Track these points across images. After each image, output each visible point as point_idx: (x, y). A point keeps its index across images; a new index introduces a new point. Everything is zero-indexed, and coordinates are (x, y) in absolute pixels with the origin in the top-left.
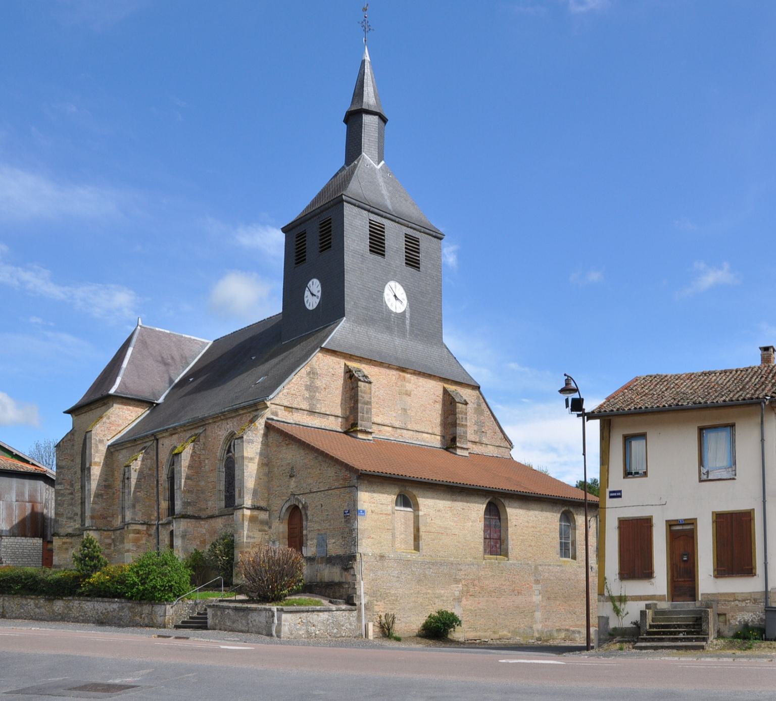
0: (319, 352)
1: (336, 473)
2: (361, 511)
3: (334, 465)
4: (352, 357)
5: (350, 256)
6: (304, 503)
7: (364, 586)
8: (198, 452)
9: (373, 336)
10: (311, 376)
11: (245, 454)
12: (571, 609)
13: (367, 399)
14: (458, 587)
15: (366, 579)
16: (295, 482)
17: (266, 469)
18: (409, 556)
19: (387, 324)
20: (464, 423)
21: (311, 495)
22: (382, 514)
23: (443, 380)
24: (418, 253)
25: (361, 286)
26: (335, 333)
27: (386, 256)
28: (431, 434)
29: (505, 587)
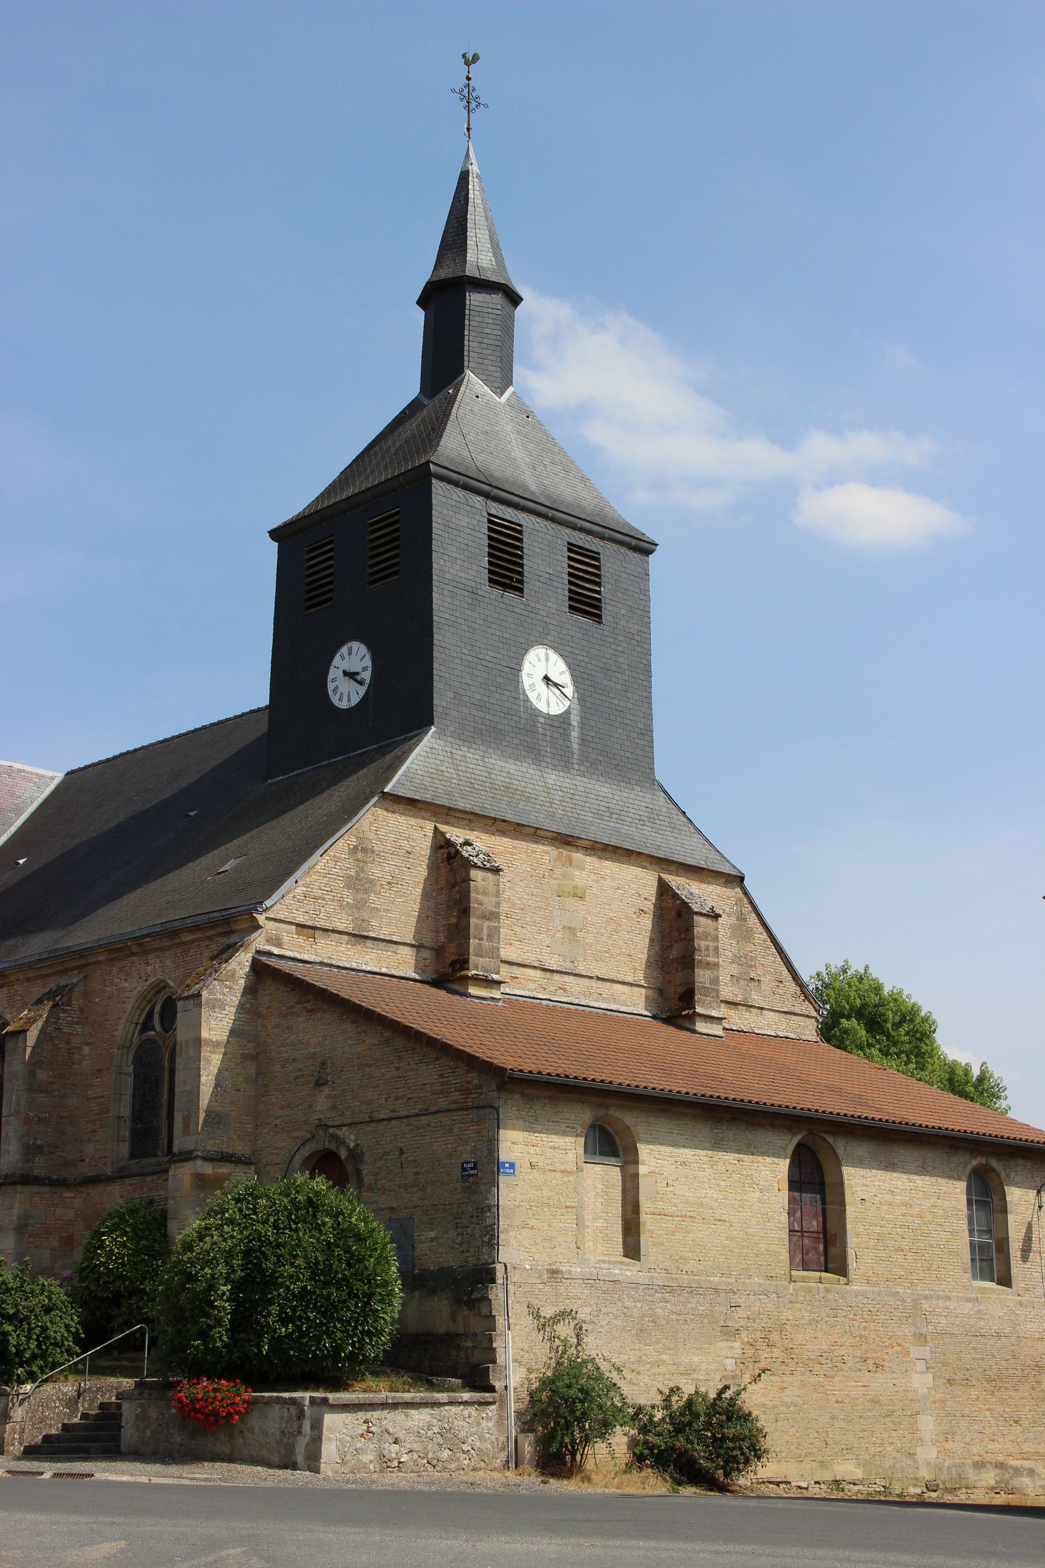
0: (374, 805)
1: (441, 1076)
2: (507, 1165)
3: (438, 1059)
4: (451, 813)
5: (446, 593)
6: (352, 1145)
7: (514, 1342)
8: (66, 1030)
9: (496, 767)
10: (360, 856)
11: (205, 1034)
12: (1007, 1409)
13: (490, 908)
14: (732, 1348)
15: (518, 1327)
16: (328, 1097)
17: (252, 1068)
18: (617, 1271)
19: (528, 739)
20: (710, 959)
21: (371, 1127)
22: (554, 1171)
23: (657, 864)
24: (599, 584)
25: (470, 658)
26: (412, 763)
27: (525, 590)
28: (632, 985)
29: (842, 1351)
